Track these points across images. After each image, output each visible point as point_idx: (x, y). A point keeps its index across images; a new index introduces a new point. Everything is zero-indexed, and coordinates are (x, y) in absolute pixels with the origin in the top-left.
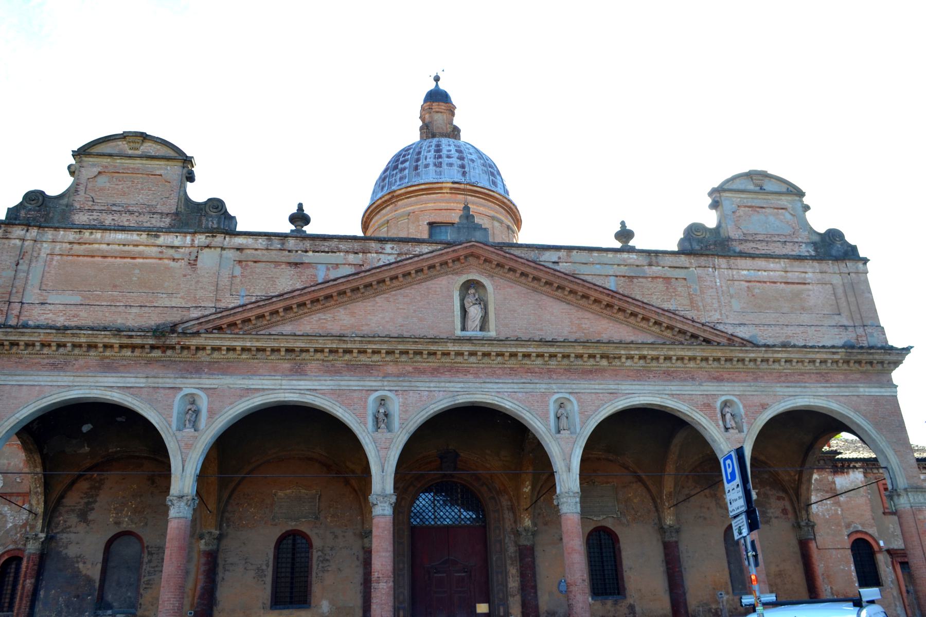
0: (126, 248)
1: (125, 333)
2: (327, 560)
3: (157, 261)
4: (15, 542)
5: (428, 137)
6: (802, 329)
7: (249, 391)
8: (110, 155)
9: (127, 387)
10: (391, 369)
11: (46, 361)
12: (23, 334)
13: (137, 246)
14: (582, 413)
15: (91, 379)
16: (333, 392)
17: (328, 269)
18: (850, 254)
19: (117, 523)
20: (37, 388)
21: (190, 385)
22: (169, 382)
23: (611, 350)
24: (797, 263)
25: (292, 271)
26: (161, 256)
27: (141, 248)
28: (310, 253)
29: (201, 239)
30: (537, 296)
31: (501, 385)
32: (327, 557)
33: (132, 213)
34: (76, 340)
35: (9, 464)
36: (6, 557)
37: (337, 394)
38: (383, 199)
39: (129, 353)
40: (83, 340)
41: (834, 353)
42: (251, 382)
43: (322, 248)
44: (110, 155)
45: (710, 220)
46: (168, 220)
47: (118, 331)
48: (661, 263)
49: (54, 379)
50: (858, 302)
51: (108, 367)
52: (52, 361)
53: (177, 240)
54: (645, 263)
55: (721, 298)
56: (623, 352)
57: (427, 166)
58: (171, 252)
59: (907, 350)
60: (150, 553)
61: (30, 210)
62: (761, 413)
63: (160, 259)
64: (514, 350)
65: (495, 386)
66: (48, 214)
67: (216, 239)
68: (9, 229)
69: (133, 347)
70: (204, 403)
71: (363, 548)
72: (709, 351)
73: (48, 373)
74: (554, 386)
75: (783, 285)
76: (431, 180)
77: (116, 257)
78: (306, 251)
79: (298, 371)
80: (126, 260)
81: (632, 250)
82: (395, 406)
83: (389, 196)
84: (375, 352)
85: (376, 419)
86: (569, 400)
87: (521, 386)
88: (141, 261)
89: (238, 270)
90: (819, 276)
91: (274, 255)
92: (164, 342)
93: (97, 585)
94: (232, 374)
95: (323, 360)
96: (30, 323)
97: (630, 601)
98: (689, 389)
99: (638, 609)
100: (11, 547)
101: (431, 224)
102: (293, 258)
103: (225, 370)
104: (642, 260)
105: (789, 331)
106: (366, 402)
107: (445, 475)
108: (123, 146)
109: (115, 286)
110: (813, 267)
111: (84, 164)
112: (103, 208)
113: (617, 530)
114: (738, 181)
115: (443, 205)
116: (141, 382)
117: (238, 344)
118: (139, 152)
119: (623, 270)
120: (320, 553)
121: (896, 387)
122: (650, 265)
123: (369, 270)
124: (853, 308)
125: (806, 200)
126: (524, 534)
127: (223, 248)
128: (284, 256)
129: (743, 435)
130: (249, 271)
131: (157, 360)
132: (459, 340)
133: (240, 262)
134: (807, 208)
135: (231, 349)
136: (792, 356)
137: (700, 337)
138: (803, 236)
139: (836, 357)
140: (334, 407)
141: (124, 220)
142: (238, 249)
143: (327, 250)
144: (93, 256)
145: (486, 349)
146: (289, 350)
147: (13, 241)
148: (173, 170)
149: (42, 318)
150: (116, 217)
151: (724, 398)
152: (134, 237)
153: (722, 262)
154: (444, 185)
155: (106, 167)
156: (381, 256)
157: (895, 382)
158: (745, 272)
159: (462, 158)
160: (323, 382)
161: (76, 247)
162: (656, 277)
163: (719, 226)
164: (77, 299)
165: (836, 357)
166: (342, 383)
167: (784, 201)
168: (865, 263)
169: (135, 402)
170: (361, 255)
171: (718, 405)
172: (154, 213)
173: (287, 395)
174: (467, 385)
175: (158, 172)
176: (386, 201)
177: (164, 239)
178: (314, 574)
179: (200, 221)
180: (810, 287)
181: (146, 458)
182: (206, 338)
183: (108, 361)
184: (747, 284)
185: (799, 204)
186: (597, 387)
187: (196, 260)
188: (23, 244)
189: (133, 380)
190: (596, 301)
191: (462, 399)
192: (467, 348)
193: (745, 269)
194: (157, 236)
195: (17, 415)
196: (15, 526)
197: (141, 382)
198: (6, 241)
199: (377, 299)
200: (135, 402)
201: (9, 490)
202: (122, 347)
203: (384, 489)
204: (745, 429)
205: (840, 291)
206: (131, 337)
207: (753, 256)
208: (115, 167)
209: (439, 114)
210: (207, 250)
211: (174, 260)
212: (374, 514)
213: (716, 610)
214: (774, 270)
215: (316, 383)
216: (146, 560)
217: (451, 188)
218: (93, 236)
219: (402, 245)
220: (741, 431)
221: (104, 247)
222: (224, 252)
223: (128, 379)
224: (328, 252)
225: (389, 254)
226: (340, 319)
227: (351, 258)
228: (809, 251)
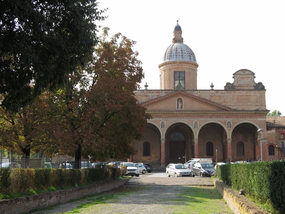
23: (206, 112)
54: (215, 93)
57: (174, 56)
76: (174, 60)
90: (254, 94)
98: (221, 119)
102: (146, 95)
105: (245, 107)
114: (239, 72)
115: (178, 67)
128: (144, 94)
180: (252, 96)
192: (178, 113)
199: (162, 103)
204: (232, 127)
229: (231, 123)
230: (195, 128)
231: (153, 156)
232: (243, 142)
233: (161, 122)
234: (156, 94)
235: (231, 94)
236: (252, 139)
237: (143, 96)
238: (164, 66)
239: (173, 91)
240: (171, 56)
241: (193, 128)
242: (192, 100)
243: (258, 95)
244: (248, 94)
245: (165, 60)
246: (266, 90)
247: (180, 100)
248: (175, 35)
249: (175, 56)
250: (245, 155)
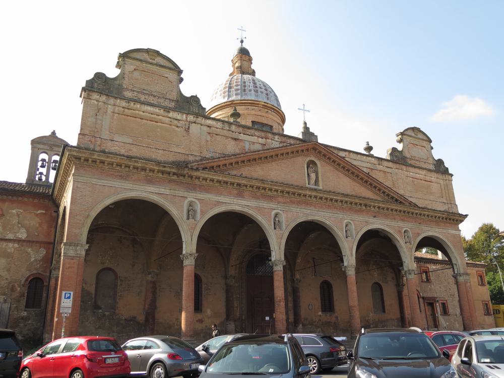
0: (153, 116)
1: (162, 164)
2: (209, 289)
3: (169, 126)
4: (36, 269)
6: (431, 202)
7: (219, 203)
8: (141, 60)
9: (160, 194)
10: (280, 199)
11: (117, 174)
12: (108, 157)
13: (158, 115)
14: (355, 230)
15: (142, 187)
16: (256, 208)
17: (250, 144)
18: (446, 171)
19: (103, 263)
20: (114, 188)
21: (191, 196)
22: (181, 193)
23: (368, 203)
24: (429, 172)
25: (233, 142)
26: (171, 123)
27: (160, 117)
28: (242, 135)
29: (191, 118)
30: (337, 172)
31: (325, 213)
32: (209, 287)
33: (155, 96)
34: (136, 164)
35: (30, 224)
36: (32, 277)
37: (258, 209)
38: (226, 104)
39: (161, 175)
40: (140, 165)
41: (443, 214)
42: (220, 198)
43: (248, 133)
44: (141, 60)
45: (112, 72)
46: (173, 104)
47: (158, 163)
48: (383, 164)
49: (123, 184)
50: (448, 193)
51: (150, 181)
52: (120, 174)
53: (179, 117)
54: (377, 163)
55: (403, 182)
56: (372, 204)
57: (250, 90)
58: (176, 122)
59: (466, 216)
60: (121, 280)
61: (99, 84)
62: (418, 237)
63: (170, 125)
64: (332, 197)
65: (323, 213)
66: (110, 88)
67: (198, 119)
68: (90, 94)
69: (163, 172)
70: (198, 207)
71: (226, 284)
72: (399, 207)
73: (119, 181)
74: (345, 216)
75: (424, 182)
76: (253, 99)
77: (147, 120)
78: (240, 133)
79: (240, 195)
80: (153, 123)
81: (372, 156)
82: (283, 218)
83: (231, 103)
84: (277, 191)
86: (350, 223)
87: (333, 214)
88: (161, 124)
89: (209, 138)
90: (436, 179)
91: (225, 133)
92: (181, 172)
93: (93, 296)
94: (211, 193)
95: (252, 191)
96: (106, 150)
97: (336, 314)
98: (393, 223)
99: (339, 318)
100: (34, 272)
101: (253, 122)
102: (235, 136)
103: (207, 190)
104: (376, 162)
105: (427, 202)
106: (271, 215)
107: (262, 251)
108: (145, 56)
109: (148, 136)
110: (434, 175)
111: (126, 63)
112: (139, 91)
113: (331, 282)
114: (409, 131)
115: (259, 113)
116: (167, 192)
117: (216, 178)
118: (155, 62)
119: (369, 165)
120: (205, 285)
121: (460, 231)
122: (379, 165)
123: (268, 149)
124: (447, 195)
126: (296, 281)
127: (202, 125)
128: (230, 134)
129: (412, 246)
130: (214, 139)
131: (174, 181)
132: (311, 189)
133: (209, 133)
135: (212, 180)
136: (429, 213)
137: (398, 200)
138: (174, 96)
139: (444, 216)
140: (257, 215)
141: (151, 99)
142: (208, 126)
143: (249, 134)
144: (136, 118)
145: (321, 195)
146: (239, 185)
147: (93, 101)
148: (172, 76)
149: (113, 148)
150: (147, 97)
151: (405, 229)
152: (157, 110)
153: (404, 167)
154: (260, 103)
155: (138, 67)
156: (273, 141)
157: (460, 229)
158: (412, 174)
159: (266, 90)
160: (252, 202)
161: (126, 110)
162: (381, 171)
163: (402, 151)
164: (129, 140)
165: (444, 216)
166: (261, 204)
168: (452, 177)
169: (165, 202)
170: (264, 139)
172: (166, 99)
173: (236, 207)
174: (312, 211)
175: (166, 76)
176: (227, 105)
177: (171, 114)
178: (203, 296)
179: (189, 108)
180: (433, 184)
181: (117, 229)
182: (201, 173)
183: (149, 178)
184: (412, 179)
185: (429, 146)
186: (361, 218)
187: (188, 129)
188: (98, 104)
189: (163, 190)
190: (362, 179)
191: (310, 218)
192: (314, 194)
193: (412, 172)
194: (169, 112)
195: (105, 202)
196: (36, 260)
197: (167, 192)
198: (89, 100)
199: (273, 163)
200: (165, 202)
201: (31, 239)
202: (158, 171)
203: (280, 258)
204: (412, 243)
205: (443, 187)
206: (165, 167)
207: (415, 167)
208: (143, 68)
209: (245, 62)
210: (194, 124)
211: (177, 127)
212: (184, 264)
213: (368, 319)
214: (421, 174)
215: (249, 202)
216: (119, 284)
217: (263, 105)
218: (135, 106)
219: (282, 137)
220: (411, 244)
221: (141, 113)
222: (202, 127)
223: (161, 189)
224: (250, 135)
225: (276, 141)
226: (258, 171)
227: (260, 140)
228: (432, 167)
229: (411, 234)
230: (347, 237)
231: (209, 312)
232: (381, 283)
233: (274, 212)
234: (260, 139)
235: (394, 169)
236: (393, 278)
237: (227, 137)
238: (228, 109)
239: (298, 142)
240: (245, 90)
241: (343, 236)
242: (337, 169)
243: (442, 182)
244: (428, 178)
245: (229, 96)
246: (452, 175)
247: (311, 164)
248: (241, 62)
249: (253, 92)
250: (386, 312)
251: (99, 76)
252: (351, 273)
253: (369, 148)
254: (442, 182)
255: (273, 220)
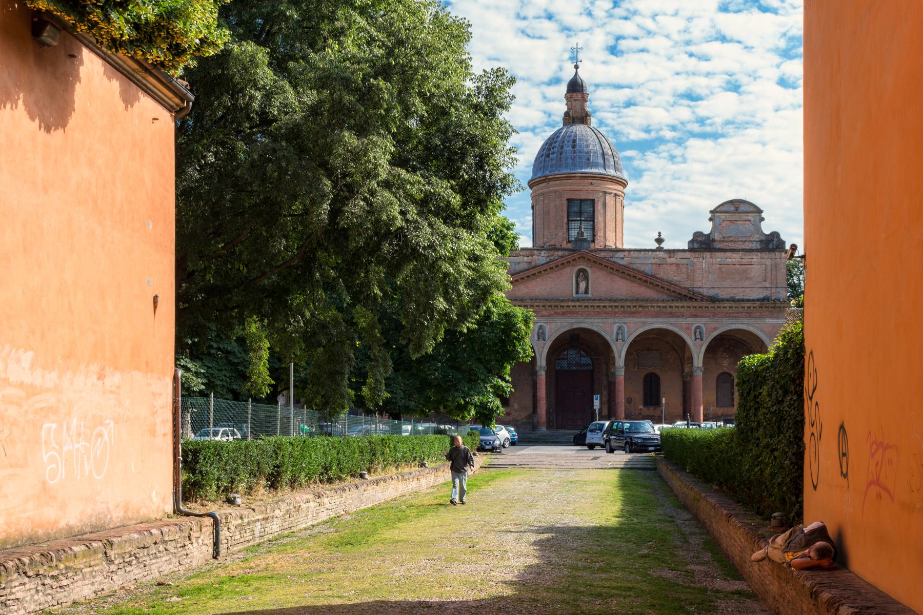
5: (569, 123)
10: (544, 313)
23: (643, 303)
45: (706, 228)
82: (547, 328)
85: (538, 335)
105: (735, 291)
125: (763, 215)
134: (763, 219)
138: (756, 237)
167: (750, 217)
171: (693, 328)
192: (577, 304)
193: (719, 257)
205: (769, 268)
231: (516, 406)
235: (705, 261)
239: (567, 253)
244: (745, 261)
251: (697, 234)
252: (621, 373)
253: (659, 241)
254: (769, 262)
255: (615, 333)
